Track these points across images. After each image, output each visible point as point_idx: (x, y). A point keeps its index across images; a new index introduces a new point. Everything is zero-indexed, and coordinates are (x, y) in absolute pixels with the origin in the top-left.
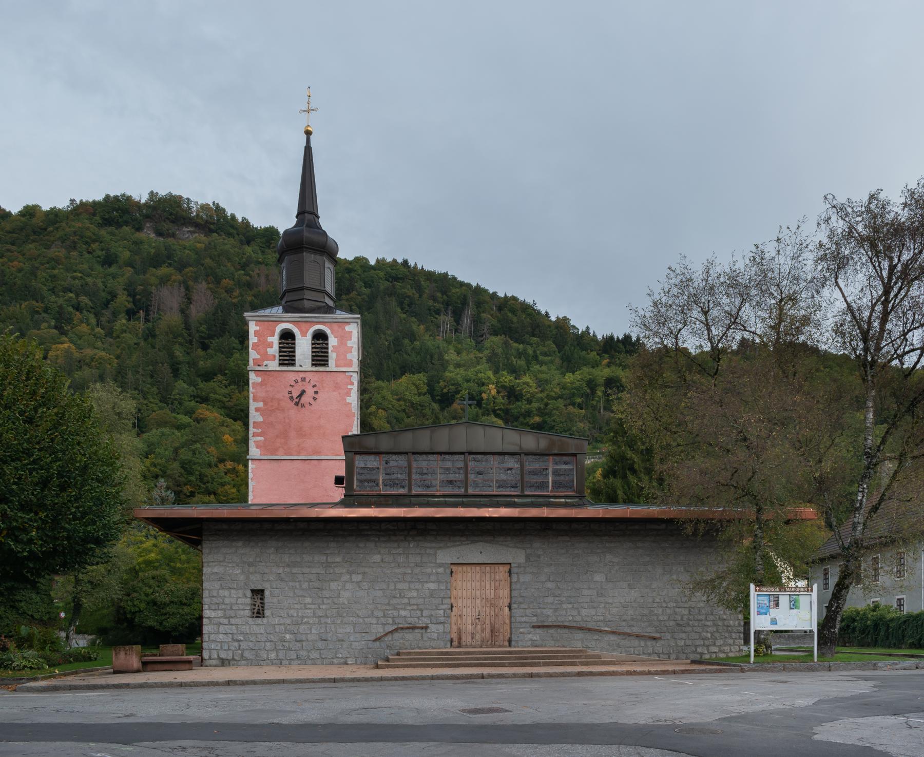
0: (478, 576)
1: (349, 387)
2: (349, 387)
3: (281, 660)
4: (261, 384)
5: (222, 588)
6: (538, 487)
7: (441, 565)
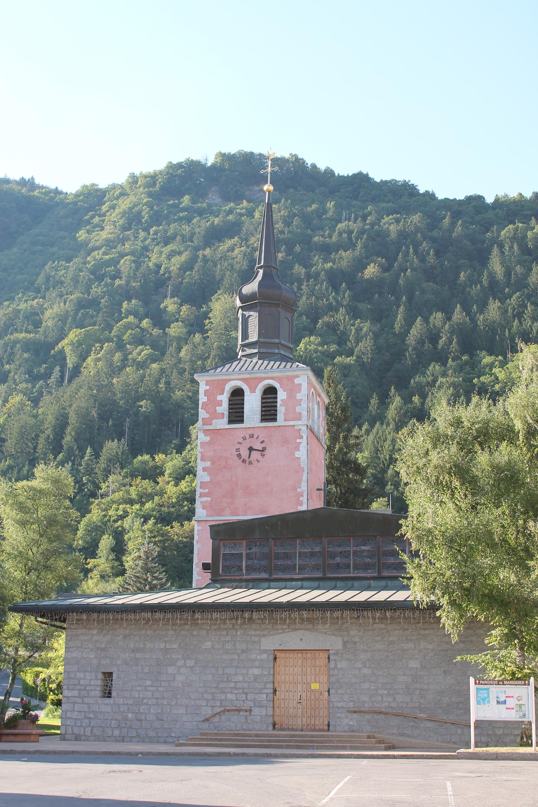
0: (300, 662)
1: (298, 441)
2: (298, 441)
4: (210, 443)
5: (79, 671)
6: (395, 568)
7: (265, 651)
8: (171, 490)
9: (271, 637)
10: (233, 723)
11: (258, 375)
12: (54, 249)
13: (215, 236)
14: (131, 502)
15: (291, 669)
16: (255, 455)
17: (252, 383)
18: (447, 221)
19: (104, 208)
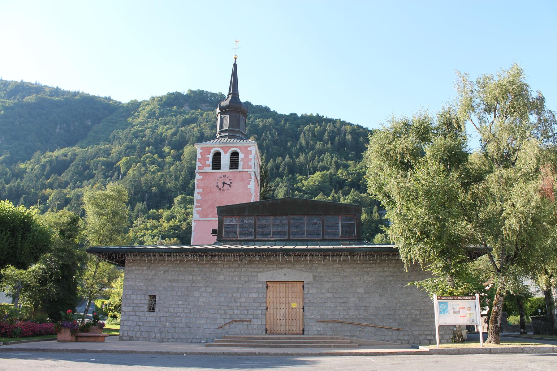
0: (284, 289)
3: (163, 338)
4: (202, 179)
5: (133, 294)
7: (260, 282)
8: (165, 225)
9: (265, 273)
10: (239, 330)
11: (229, 145)
12: (118, 125)
13: (186, 122)
14: (148, 229)
15: (278, 294)
16: (226, 186)
17: (226, 149)
18: (282, 122)
19: (140, 109)
